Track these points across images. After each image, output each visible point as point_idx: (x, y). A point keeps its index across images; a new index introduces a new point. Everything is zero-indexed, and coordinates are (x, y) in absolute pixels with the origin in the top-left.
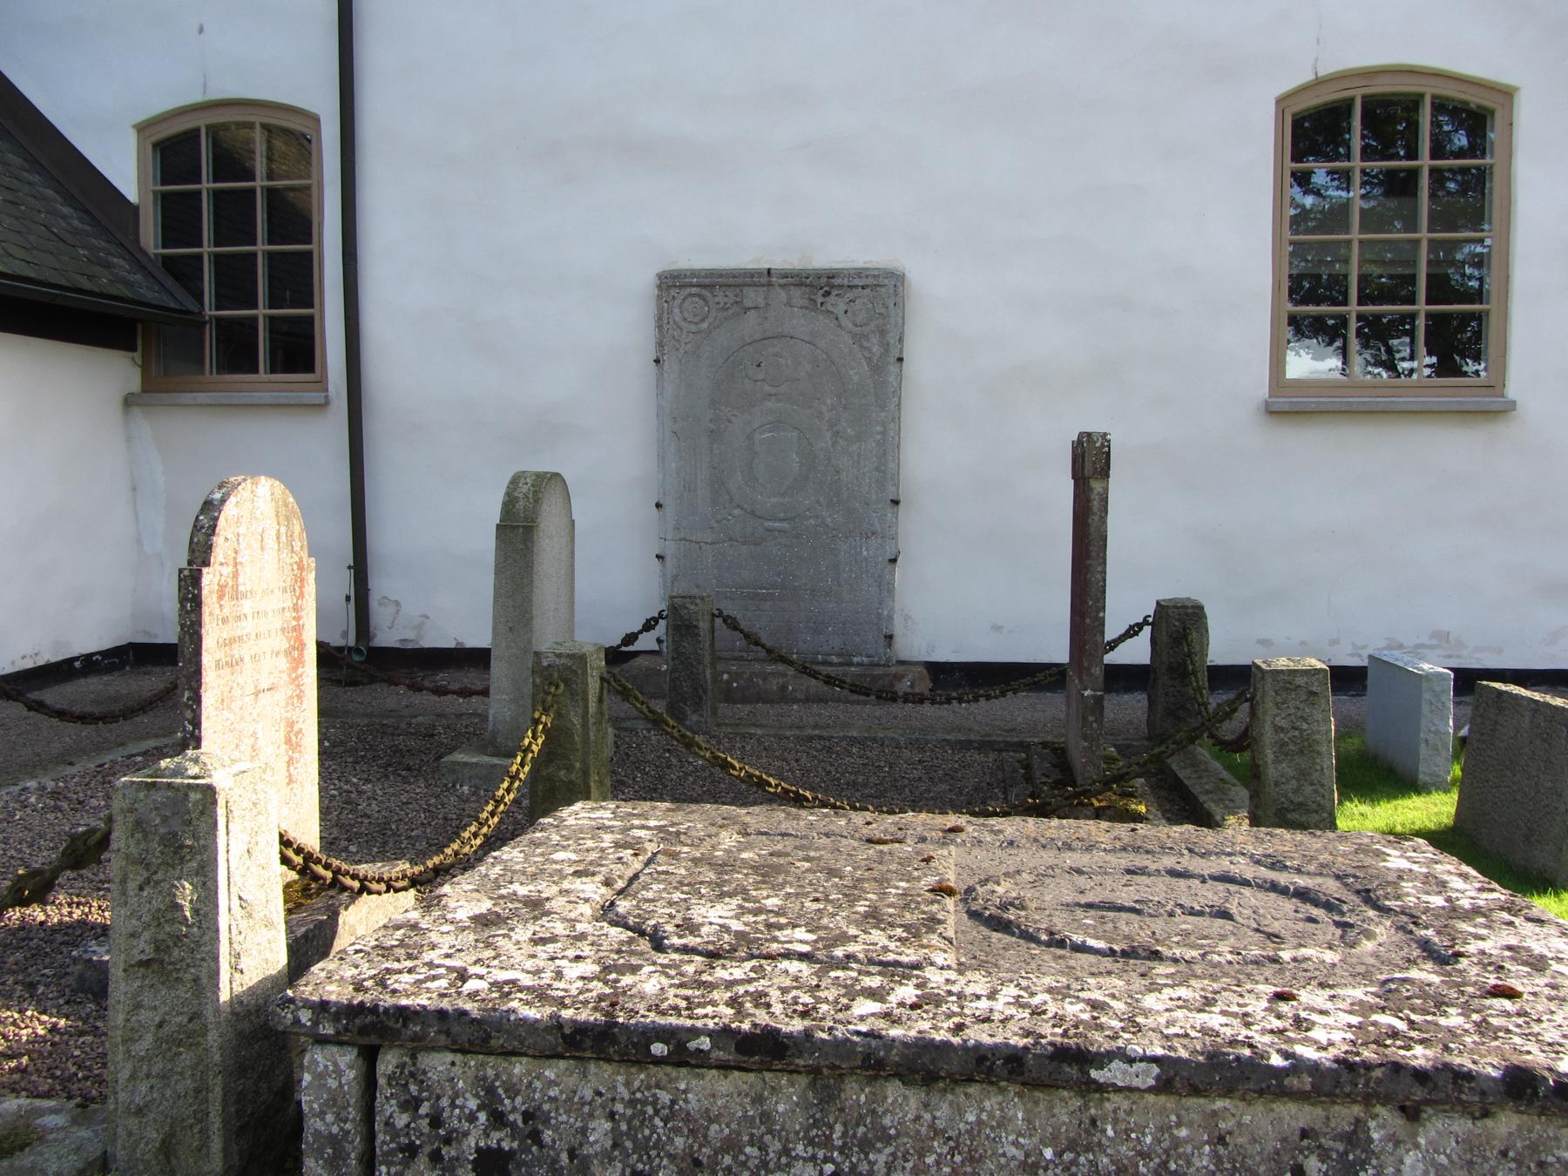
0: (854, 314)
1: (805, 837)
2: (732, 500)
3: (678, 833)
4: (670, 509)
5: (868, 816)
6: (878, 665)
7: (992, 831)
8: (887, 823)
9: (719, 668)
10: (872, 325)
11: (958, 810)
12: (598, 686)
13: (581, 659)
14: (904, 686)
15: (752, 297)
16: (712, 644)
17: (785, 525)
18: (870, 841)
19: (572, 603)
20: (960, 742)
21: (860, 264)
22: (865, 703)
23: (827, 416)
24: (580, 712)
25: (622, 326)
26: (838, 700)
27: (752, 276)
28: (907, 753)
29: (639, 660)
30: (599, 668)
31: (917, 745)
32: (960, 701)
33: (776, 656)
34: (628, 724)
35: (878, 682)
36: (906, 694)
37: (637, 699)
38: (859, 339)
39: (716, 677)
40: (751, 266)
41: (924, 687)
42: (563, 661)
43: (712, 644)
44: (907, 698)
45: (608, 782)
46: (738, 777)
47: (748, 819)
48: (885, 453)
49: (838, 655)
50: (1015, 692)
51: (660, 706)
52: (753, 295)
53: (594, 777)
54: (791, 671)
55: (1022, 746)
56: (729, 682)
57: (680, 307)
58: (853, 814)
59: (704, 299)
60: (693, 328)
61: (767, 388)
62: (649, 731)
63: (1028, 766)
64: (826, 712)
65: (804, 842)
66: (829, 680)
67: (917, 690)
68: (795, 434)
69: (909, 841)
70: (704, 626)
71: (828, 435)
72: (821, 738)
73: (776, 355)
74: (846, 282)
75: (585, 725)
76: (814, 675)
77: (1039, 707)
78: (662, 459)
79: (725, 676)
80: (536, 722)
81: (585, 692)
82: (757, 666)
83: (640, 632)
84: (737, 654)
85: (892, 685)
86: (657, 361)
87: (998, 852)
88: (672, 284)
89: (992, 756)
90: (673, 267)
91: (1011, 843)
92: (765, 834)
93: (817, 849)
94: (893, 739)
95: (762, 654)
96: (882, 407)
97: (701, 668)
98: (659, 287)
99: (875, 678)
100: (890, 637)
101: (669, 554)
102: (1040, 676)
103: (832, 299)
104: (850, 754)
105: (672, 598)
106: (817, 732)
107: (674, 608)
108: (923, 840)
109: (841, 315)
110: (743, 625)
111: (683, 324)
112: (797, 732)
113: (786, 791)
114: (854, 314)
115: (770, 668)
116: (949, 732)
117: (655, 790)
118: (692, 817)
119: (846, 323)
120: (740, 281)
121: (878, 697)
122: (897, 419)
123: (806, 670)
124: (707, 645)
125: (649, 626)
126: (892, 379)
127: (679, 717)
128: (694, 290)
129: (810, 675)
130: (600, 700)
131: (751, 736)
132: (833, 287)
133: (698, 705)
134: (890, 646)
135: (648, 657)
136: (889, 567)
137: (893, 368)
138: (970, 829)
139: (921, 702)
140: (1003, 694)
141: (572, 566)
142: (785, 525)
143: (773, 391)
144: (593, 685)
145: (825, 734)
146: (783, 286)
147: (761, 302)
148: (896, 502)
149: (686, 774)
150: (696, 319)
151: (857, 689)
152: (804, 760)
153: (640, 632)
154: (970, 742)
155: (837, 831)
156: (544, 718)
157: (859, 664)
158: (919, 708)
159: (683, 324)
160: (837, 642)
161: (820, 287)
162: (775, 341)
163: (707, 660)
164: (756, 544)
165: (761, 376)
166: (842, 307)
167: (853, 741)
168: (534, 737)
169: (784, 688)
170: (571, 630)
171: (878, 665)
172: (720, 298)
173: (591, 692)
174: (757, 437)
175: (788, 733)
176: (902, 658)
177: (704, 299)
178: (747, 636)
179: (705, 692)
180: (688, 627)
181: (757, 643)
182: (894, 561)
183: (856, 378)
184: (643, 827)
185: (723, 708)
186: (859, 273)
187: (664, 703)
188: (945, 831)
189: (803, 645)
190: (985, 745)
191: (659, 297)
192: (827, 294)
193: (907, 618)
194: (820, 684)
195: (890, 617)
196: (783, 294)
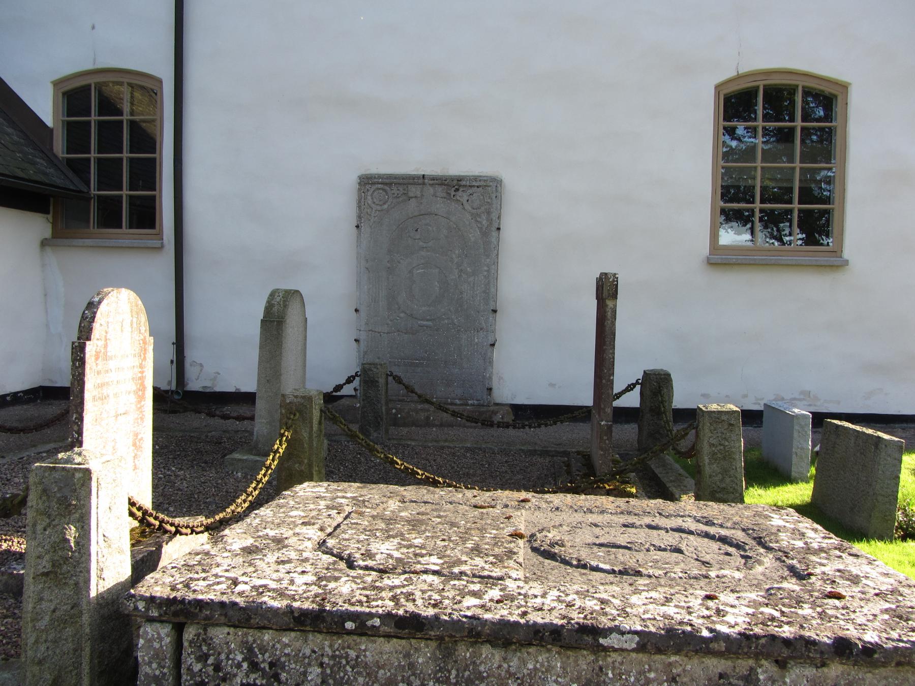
1: (438, 504)
2: (399, 308)
3: (364, 501)
4: (363, 313)
6: (483, 406)
7: (546, 502)
8: (485, 497)
9: (390, 406)
12: (319, 415)
13: (309, 399)
14: (498, 418)
15: (414, 191)
17: (430, 323)
18: (475, 507)
20: (530, 451)
21: (477, 174)
22: (475, 427)
23: (456, 260)
24: (308, 430)
25: (338, 205)
26: (460, 426)
27: (414, 179)
28: (499, 457)
30: (319, 404)
34: (337, 438)
35: (484, 415)
36: (499, 422)
38: (475, 216)
41: (509, 418)
42: (299, 400)
45: (323, 471)
47: (405, 493)
48: (489, 283)
51: (355, 428)
54: (432, 408)
55: (566, 454)
56: (396, 414)
60: (379, 208)
61: (421, 243)
62: (348, 442)
65: (437, 507)
66: (454, 414)
67: (505, 420)
68: (437, 270)
70: (382, 381)
71: (456, 271)
73: (427, 224)
74: (468, 184)
76: (446, 411)
78: (359, 283)
79: (394, 411)
80: (282, 435)
81: (311, 419)
83: (344, 384)
84: (401, 398)
85: (491, 417)
86: (357, 227)
87: (550, 514)
88: (367, 182)
89: (548, 460)
90: (368, 172)
91: (557, 509)
92: (415, 502)
93: (445, 511)
95: (416, 398)
96: (488, 256)
98: (360, 184)
100: (490, 390)
102: (576, 413)
103: (460, 193)
104: (465, 457)
106: (447, 444)
108: (506, 506)
109: (465, 202)
112: (435, 444)
114: (472, 202)
118: (372, 491)
119: (467, 206)
121: (483, 424)
122: (496, 263)
123: (441, 408)
125: (349, 380)
126: (494, 240)
127: (366, 433)
128: (380, 186)
129: (443, 410)
130: (320, 423)
131: (408, 446)
132: (460, 186)
134: (490, 395)
135: (348, 399)
137: (495, 234)
138: (534, 500)
139: (508, 427)
140: (555, 423)
142: (430, 323)
143: (425, 245)
144: (316, 414)
147: (418, 194)
148: (495, 311)
149: (370, 468)
150: (381, 203)
151: (470, 419)
153: (344, 384)
154: (535, 451)
156: (286, 433)
157: (472, 405)
158: (506, 430)
161: (453, 186)
163: (383, 402)
165: (418, 237)
166: (465, 198)
167: (468, 449)
169: (428, 418)
170: (304, 383)
171: (483, 406)
172: (395, 191)
175: (430, 444)
178: (407, 387)
179: (382, 420)
181: (413, 391)
182: (493, 345)
183: (473, 239)
184: (343, 497)
185: (392, 429)
186: (476, 178)
190: (545, 453)
191: (359, 190)
192: (457, 190)
193: (500, 378)
195: (490, 378)
196: (431, 190)
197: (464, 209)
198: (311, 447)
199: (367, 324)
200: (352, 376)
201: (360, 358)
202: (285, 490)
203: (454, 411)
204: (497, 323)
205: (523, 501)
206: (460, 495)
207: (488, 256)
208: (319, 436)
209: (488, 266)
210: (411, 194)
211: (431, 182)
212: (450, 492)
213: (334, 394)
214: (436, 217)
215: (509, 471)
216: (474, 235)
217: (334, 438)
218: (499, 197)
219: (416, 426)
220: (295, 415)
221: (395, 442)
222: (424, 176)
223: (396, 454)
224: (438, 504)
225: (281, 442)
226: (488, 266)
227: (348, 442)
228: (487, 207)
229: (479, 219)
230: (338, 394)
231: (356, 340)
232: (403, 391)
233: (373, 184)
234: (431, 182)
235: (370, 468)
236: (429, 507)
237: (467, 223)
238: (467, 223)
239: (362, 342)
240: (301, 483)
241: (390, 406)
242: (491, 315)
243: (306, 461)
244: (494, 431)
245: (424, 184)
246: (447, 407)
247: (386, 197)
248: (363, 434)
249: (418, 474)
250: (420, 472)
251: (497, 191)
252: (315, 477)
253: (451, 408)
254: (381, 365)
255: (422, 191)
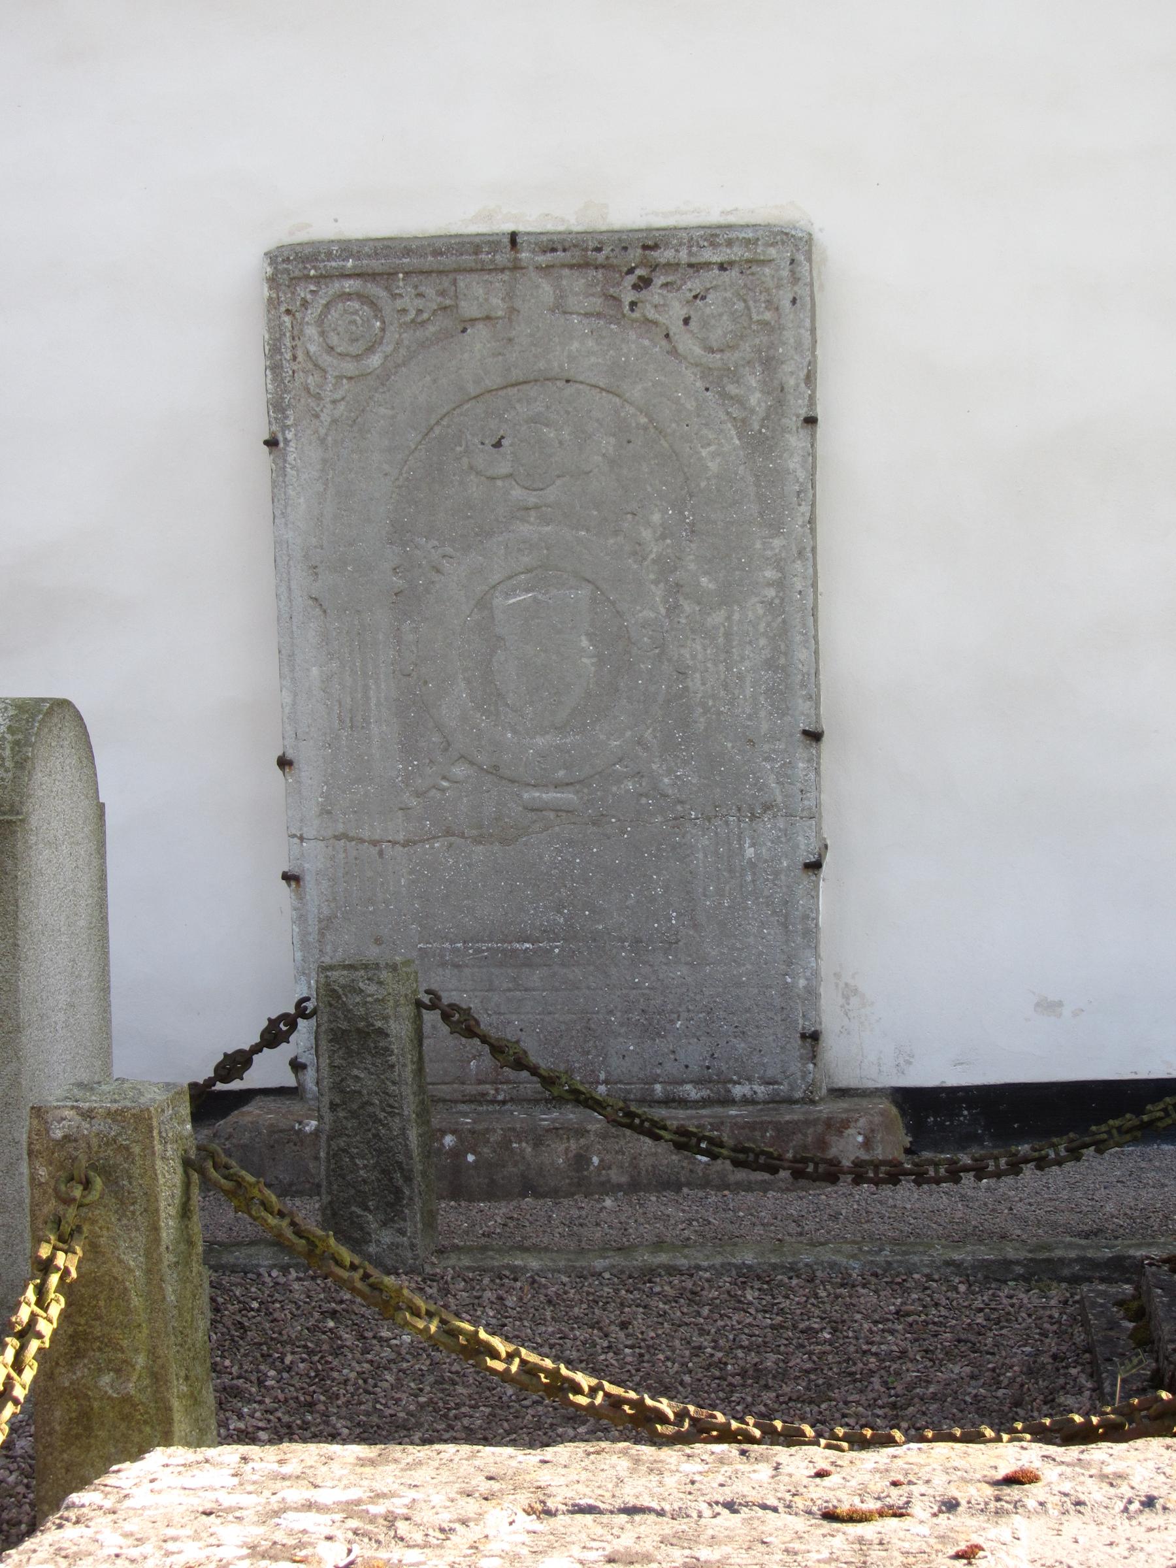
0: (705, 324)
1: (679, 1514)
2: (447, 745)
3: (391, 1519)
4: (309, 771)
5: (820, 1455)
6: (791, 1101)
7: (1103, 1477)
8: (860, 1473)
9: (435, 1122)
10: (746, 346)
11: (1004, 1426)
12: (178, 1179)
13: (141, 1120)
14: (849, 1147)
15: (478, 295)
16: (420, 1071)
17: (567, 797)
18: (830, 1516)
19: (104, 988)
20: (985, 1265)
21: (714, 217)
22: (765, 1187)
23: (655, 550)
24: (140, 1239)
25: (203, 365)
26: (705, 1184)
27: (477, 250)
28: (867, 1297)
29: (252, 1111)
30: (179, 1138)
31: (891, 1278)
32: (980, 1172)
33: (557, 1089)
34: (238, 1256)
35: (782, 1138)
36: (858, 1164)
37: (265, 1205)
38: (718, 380)
39: (430, 1150)
40: (472, 229)
41: (893, 1144)
42: (99, 1125)
43: (420, 1071)
44: (859, 1174)
45: (209, 1397)
46: (505, 1376)
47: (544, 1476)
48: (784, 631)
49: (697, 1082)
50: (1101, 1147)
51: (308, 1212)
52: (480, 291)
53: (178, 1387)
54: (596, 1122)
55: (1121, 1268)
56: (457, 1154)
57: (320, 321)
58: (781, 1453)
59: (372, 303)
60: (349, 367)
61: (517, 493)
62: (285, 1270)
63: (1140, 1314)
64: (672, 1212)
65: (681, 1525)
66: (685, 1141)
67: (880, 1153)
68: (584, 592)
69: (917, 1509)
70: (399, 1029)
71: (658, 592)
72: (672, 1270)
73: (534, 420)
74: (683, 256)
75: (152, 1270)
76: (653, 1130)
77: (1150, 1176)
78: (288, 658)
79: (449, 1140)
80: (46, 1267)
81: (151, 1196)
82: (519, 1114)
83: (257, 1049)
84: (472, 1089)
85: (823, 1144)
86: (272, 443)
87: (1125, 1528)
88: (302, 274)
89: (1057, 1292)
90: (302, 237)
91: (1149, 1502)
92: (590, 1510)
93: (713, 1541)
94: (833, 1265)
95: (530, 1085)
96: (776, 527)
97: (395, 1124)
98: (272, 281)
99: (784, 1131)
100: (813, 1038)
101: (309, 869)
102: (1154, 1111)
103: (654, 294)
104: (741, 1305)
105: (324, 969)
106: (663, 1258)
107: (331, 994)
108: (951, 1506)
109: (676, 327)
110: (487, 1022)
111: (326, 360)
112: (618, 1260)
113: (615, 1403)
114: (705, 324)
115: (547, 1118)
116: (958, 1243)
117: (311, 1405)
118: (419, 1475)
119: (687, 343)
120: (448, 261)
121: (798, 1174)
122: (808, 552)
123: (630, 1119)
124: (408, 1073)
125: (273, 1035)
126: (794, 463)
127: (356, 1239)
128: (349, 285)
129: (640, 1130)
130: (185, 1212)
131: (516, 1273)
132: (655, 267)
133: (393, 1205)
134: (813, 1057)
135: (270, 1103)
136: (806, 880)
137: (796, 441)
138: (1050, 1473)
139: (893, 1179)
140: (1075, 1154)
141: (102, 905)
142: (567, 797)
143: (532, 499)
144: (168, 1178)
145: (682, 1262)
146: (546, 270)
147: (498, 305)
148: (815, 736)
149: (379, 1368)
150: (354, 349)
151: (744, 1157)
152: (638, 1323)
153: (257, 1049)
154: (1007, 1264)
155: (753, 1496)
156: (61, 1259)
157: (747, 1101)
158: (886, 1191)
159: (326, 360)
160: (694, 1054)
161: (628, 267)
162: (532, 391)
163: (409, 1109)
164: (504, 841)
165: (504, 468)
166: (678, 310)
167: (745, 1275)
168: (42, 1302)
169: (580, 1160)
170: (105, 1052)
171: (791, 1101)
172: (408, 301)
173: (164, 1194)
174: (498, 601)
175: (599, 1264)
176: (843, 1083)
177: (372, 303)
178: (497, 1049)
179: (408, 1179)
180: (364, 1034)
181: (520, 1064)
182: (815, 866)
183: (713, 466)
184: (309, 1506)
185: (451, 1214)
186: (714, 235)
187: (315, 1204)
188: (996, 1483)
189: (619, 1063)
190: (1040, 1271)
191: (272, 303)
192: (644, 283)
193: (849, 992)
194: (662, 1148)
195: (812, 993)
196: (546, 289)
197: (674, 352)
198: (155, 1301)
199: (326, 812)
200: (284, 1017)
201: (305, 945)
202: (78, 1489)
203: (682, 1132)
204: (825, 783)
205: (1012, 1480)
206: (764, 1471)
207: (776, 527)
208: (183, 1262)
209: (779, 564)
210: (469, 309)
211: (542, 259)
212: (722, 1461)
213: (220, 1086)
214: (570, 389)
215: (913, 1351)
216: (717, 451)
217: (228, 1258)
218: (804, 302)
219: (538, 1195)
220: (87, 1185)
221: (466, 1261)
222: (513, 236)
223: (472, 1310)
224: (679, 1514)
225: (41, 1292)
226: (779, 564)
227: (285, 1270)
228: (762, 339)
229: (732, 389)
230: (236, 1085)
231: (287, 877)
232: (480, 1062)
233: (324, 278)
234: (542, 259)
235: (379, 1368)
236: (648, 1526)
237: (690, 405)
238: (690, 405)
239: (309, 881)
240: (136, 1453)
241: (435, 1122)
242: (801, 752)
243: (141, 1360)
244: (843, 1199)
245: (516, 267)
246: (659, 1113)
247: (365, 317)
248: (344, 1237)
249: (578, 1390)
250: (584, 1380)
251: (795, 279)
252: (181, 1425)
253: (676, 1117)
254: (394, 968)
255: (510, 296)
